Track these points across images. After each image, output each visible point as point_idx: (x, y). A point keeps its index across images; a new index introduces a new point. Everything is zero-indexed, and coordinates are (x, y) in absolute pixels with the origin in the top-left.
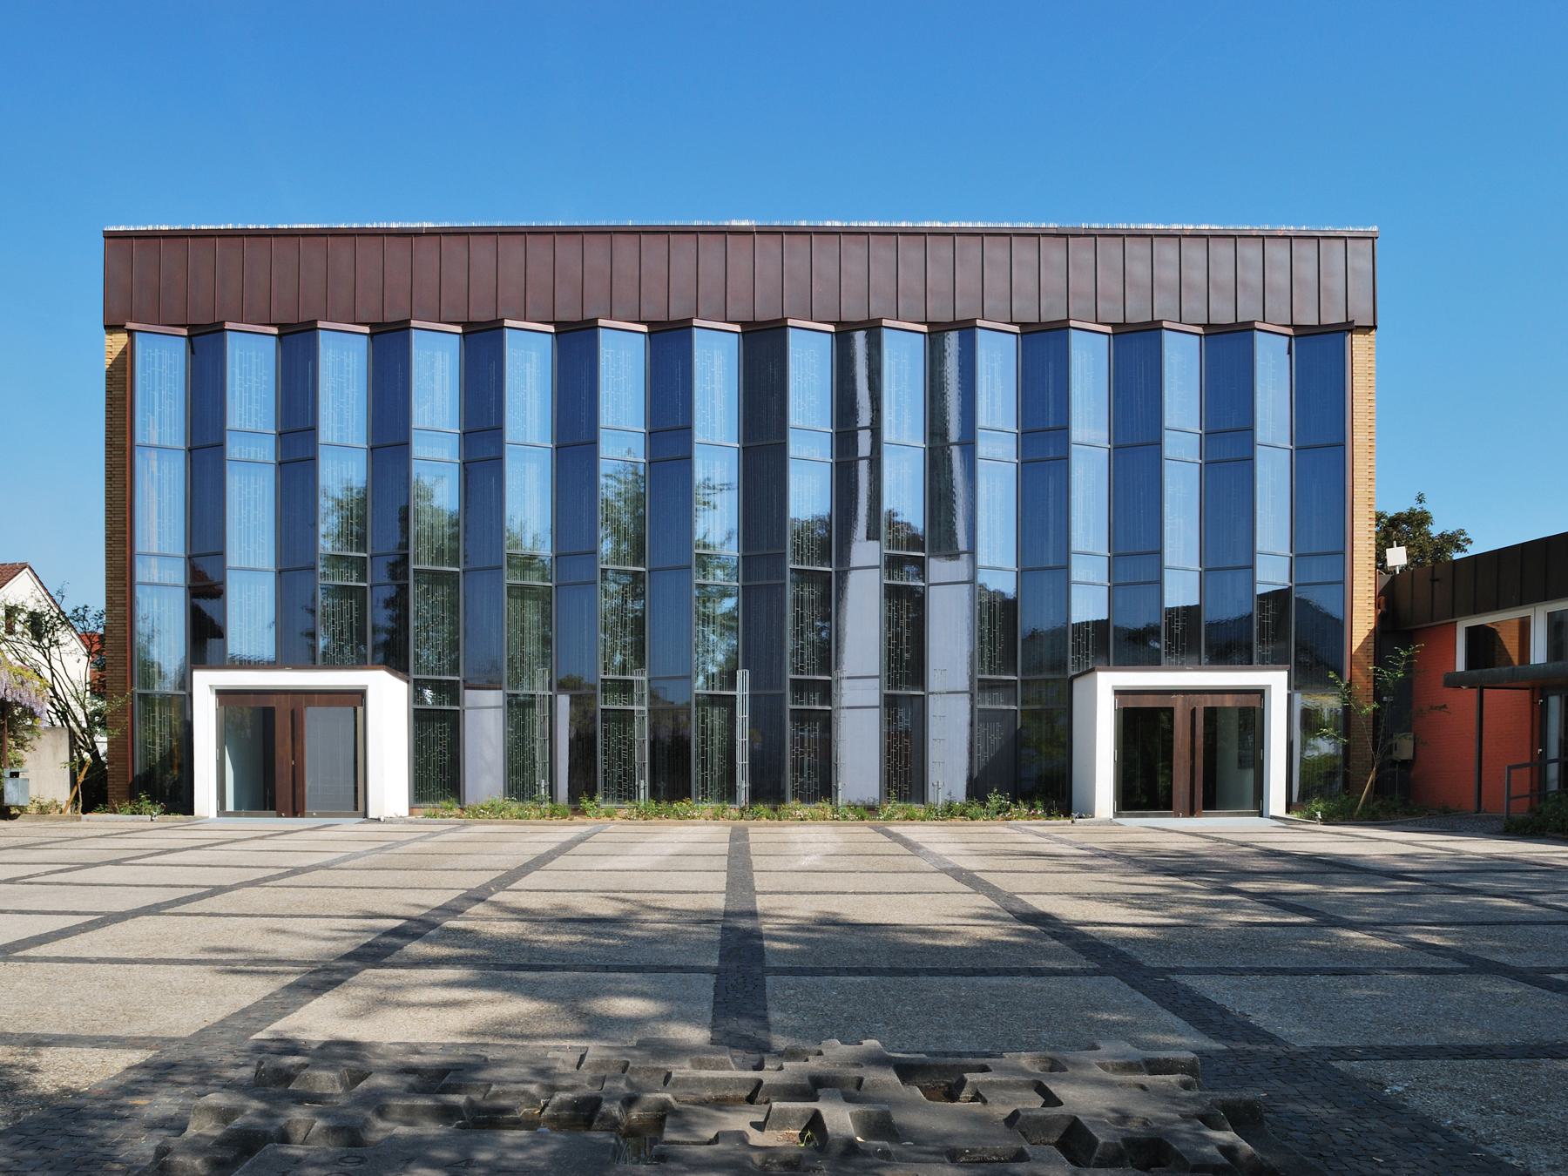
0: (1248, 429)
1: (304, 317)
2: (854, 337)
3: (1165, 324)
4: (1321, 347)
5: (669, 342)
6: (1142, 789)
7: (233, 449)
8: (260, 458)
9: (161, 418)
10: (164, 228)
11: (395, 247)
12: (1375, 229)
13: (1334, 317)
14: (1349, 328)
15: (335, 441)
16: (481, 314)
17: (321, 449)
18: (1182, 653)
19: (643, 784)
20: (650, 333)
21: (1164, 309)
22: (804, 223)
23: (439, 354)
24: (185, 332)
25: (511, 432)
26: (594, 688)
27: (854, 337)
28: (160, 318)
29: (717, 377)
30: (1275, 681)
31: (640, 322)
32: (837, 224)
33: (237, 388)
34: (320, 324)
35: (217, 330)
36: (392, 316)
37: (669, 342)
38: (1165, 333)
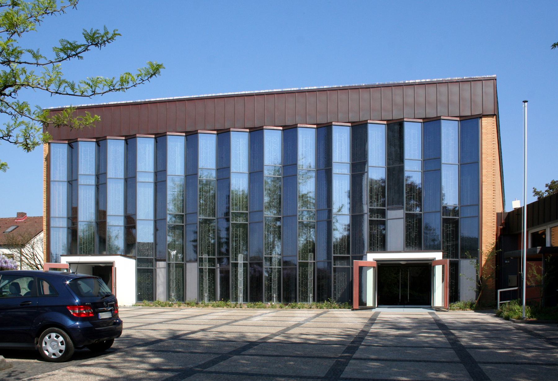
0: (438, 159)
1: (227, 127)
2: (431, 125)
3: (442, 118)
4: (469, 124)
5: (324, 133)
6: (386, 298)
7: (139, 178)
8: (91, 183)
9: (60, 172)
10: (325, 87)
11: (210, 102)
12: (495, 76)
13: (478, 112)
14: (481, 116)
15: (114, 177)
16: (289, 123)
17: (108, 180)
18: (415, 246)
19: (241, 295)
20: (250, 132)
21: (442, 111)
22: (139, 101)
23: (147, 145)
24: (67, 142)
25: (233, 169)
26: (296, 265)
27: (431, 125)
28: (59, 139)
29: (241, 148)
30: (438, 256)
31: (349, 122)
32: (295, 89)
33: (83, 161)
34: (231, 129)
35: (164, 135)
36: (257, 124)
37: (324, 133)
38: (442, 121)
